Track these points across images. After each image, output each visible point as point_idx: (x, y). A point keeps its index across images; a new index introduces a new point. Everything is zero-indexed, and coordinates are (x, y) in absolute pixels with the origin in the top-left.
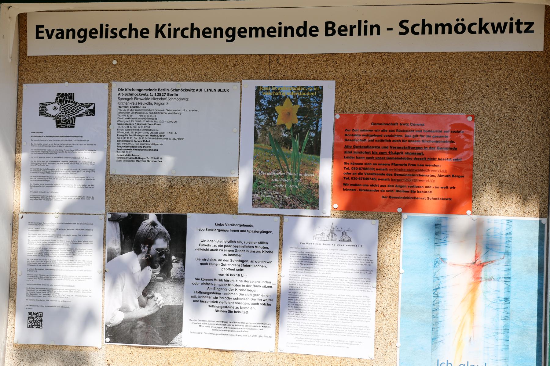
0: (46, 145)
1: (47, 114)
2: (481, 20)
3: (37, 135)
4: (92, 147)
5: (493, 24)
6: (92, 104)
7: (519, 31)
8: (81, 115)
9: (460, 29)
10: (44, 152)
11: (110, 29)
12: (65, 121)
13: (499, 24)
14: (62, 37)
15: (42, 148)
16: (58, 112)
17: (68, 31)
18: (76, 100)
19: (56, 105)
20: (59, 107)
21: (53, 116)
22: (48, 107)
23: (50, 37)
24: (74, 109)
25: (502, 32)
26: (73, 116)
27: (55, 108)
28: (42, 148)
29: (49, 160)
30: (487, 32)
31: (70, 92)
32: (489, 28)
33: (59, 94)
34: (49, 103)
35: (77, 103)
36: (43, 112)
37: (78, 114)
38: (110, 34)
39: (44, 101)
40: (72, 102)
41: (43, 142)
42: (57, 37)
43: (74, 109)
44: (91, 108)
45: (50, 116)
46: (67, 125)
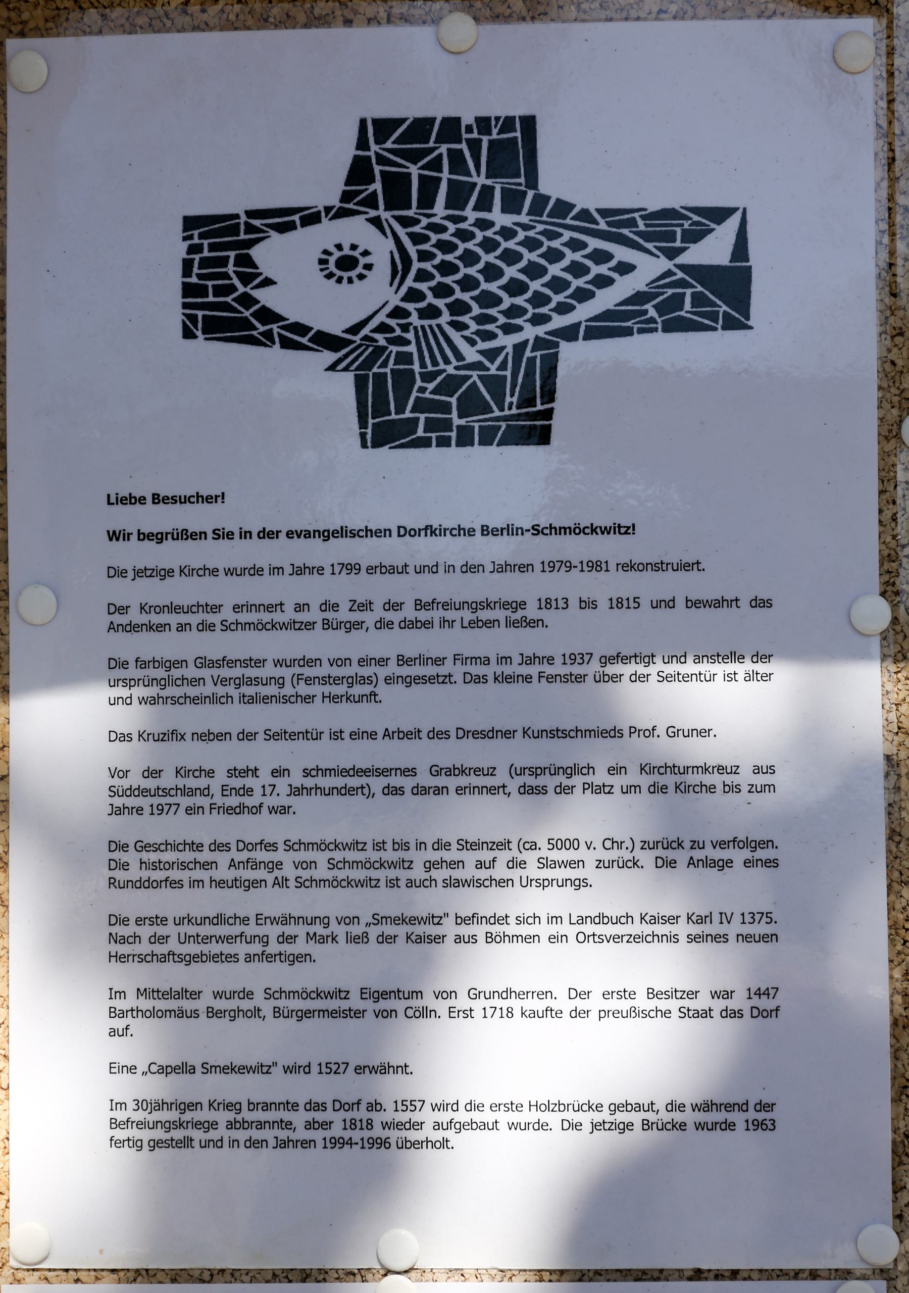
0: (264, 617)
1: (267, 315)
2: (592, 525)
3: (156, 520)
4: (740, 623)
5: (601, 528)
6: (720, 215)
7: (620, 533)
8: (608, 326)
9: (577, 531)
10: (244, 681)
11: (349, 530)
12: (450, 385)
13: (606, 528)
14: (310, 537)
15: (216, 645)
16: (375, 294)
17: (314, 531)
18: (554, 181)
19: (355, 231)
20: (381, 249)
21: (325, 341)
22: (269, 254)
23: (299, 537)
24: (534, 271)
25: (609, 533)
26: (530, 332)
27: (346, 263)
28: (216, 645)
29: (299, 756)
30: (597, 534)
31: (497, 109)
32: (598, 530)
33: (384, 127)
34: (284, 220)
35: (563, 208)
36: (222, 296)
37: (583, 312)
38: (349, 534)
39: (231, 195)
40: (512, 203)
41: (227, 592)
42: (305, 537)
43: (534, 271)
44: (714, 250)
45: (297, 337)
46: (476, 423)
